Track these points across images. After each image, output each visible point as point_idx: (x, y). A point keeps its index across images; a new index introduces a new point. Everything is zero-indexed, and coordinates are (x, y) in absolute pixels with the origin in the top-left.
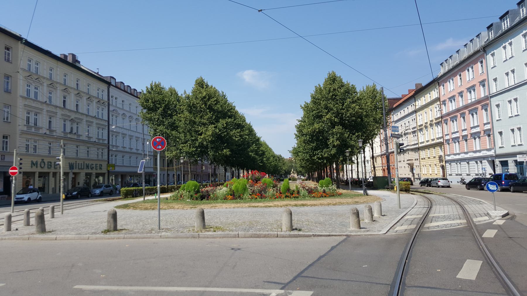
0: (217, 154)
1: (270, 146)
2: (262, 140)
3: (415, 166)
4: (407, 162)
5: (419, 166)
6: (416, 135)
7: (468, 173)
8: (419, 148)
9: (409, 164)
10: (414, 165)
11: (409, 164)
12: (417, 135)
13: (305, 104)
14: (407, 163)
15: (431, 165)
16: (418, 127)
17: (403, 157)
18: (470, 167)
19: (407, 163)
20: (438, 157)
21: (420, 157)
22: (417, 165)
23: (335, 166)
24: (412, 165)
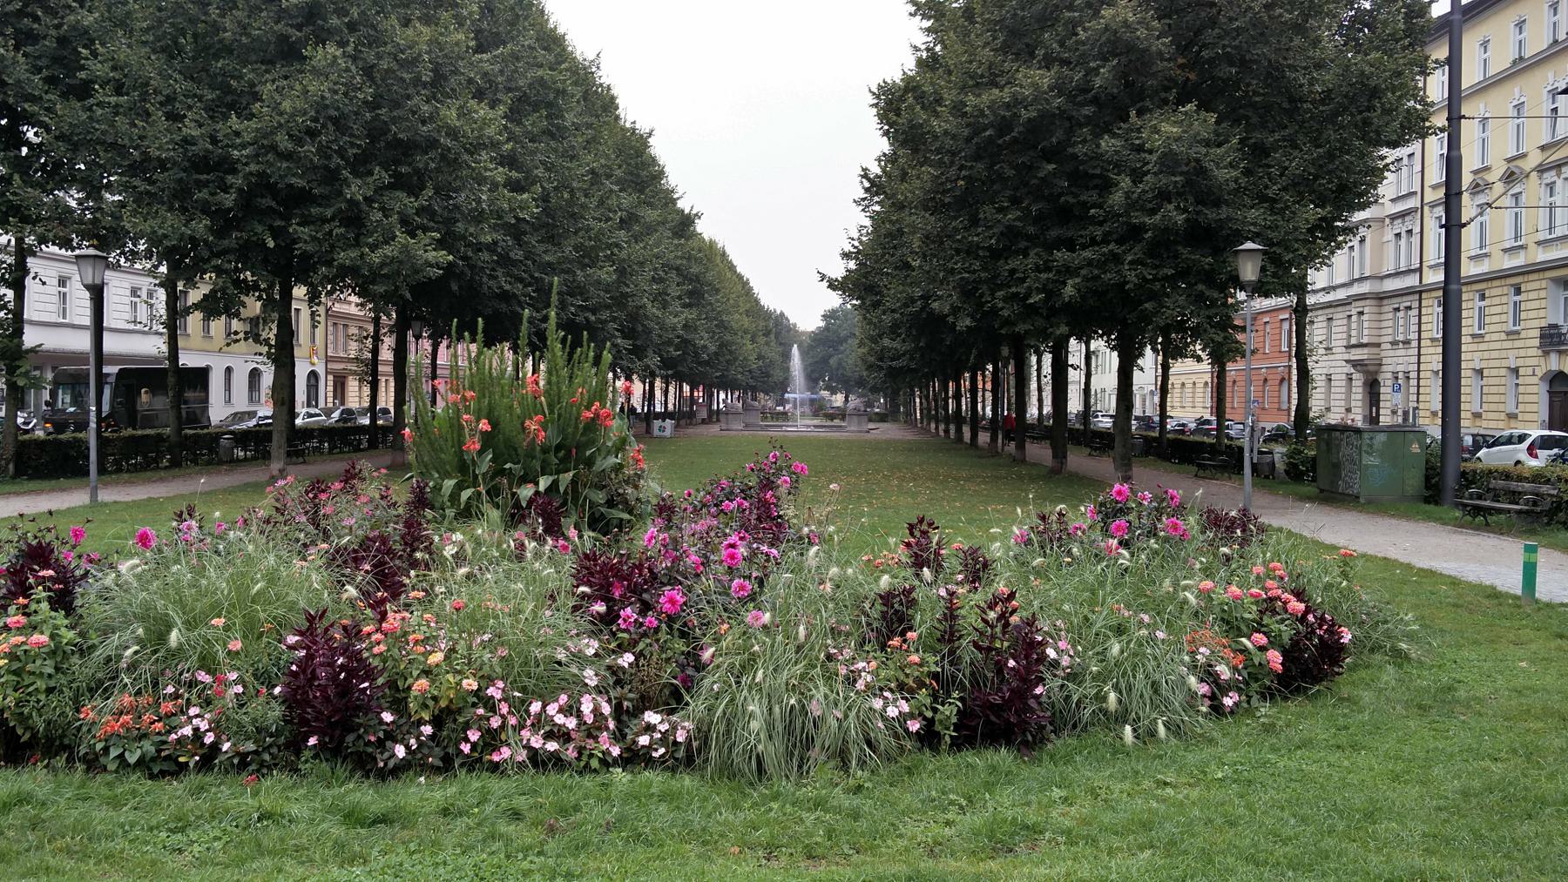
0: (25, 150)
1: (633, 111)
2: (701, 227)
3: (1389, 375)
4: (1346, 357)
5: (1413, 375)
6: (1410, 232)
7: (1511, 408)
8: (1420, 292)
9: (1356, 364)
10: (1384, 368)
11: (1356, 364)
12: (1417, 229)
13: (918, 18)
14: (1347, 361)
15: (1486, 373)
16: (1427, 190)
17: (1390, 323)
18: (1333, 390)
19: (1347, 361)
20: (1537, 333)
21: (1424, 335)
22: (1400, 368)
23: (838, 400)
24: (1371, 368)
